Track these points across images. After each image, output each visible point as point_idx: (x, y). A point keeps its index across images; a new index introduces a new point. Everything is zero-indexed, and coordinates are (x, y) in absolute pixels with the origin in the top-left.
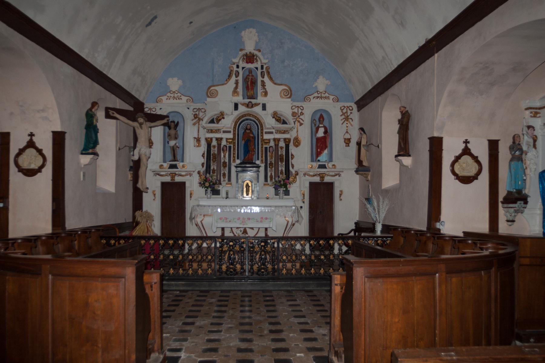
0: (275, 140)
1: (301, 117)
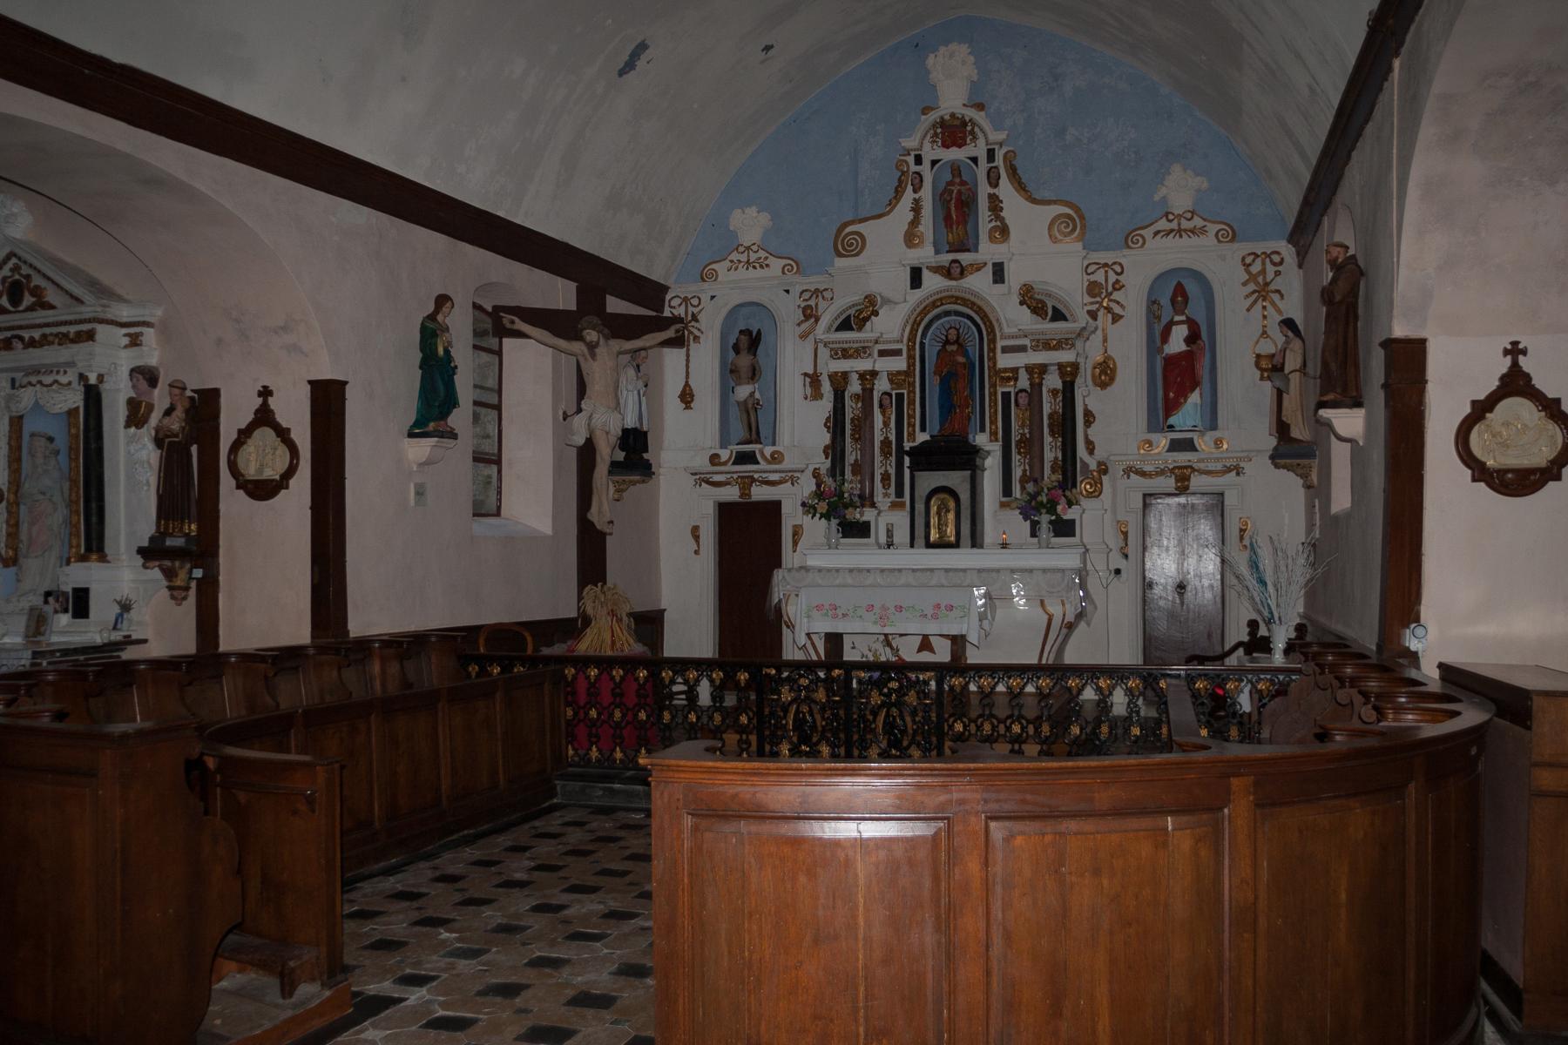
0: (1030, 369)
1: (1116, 296)
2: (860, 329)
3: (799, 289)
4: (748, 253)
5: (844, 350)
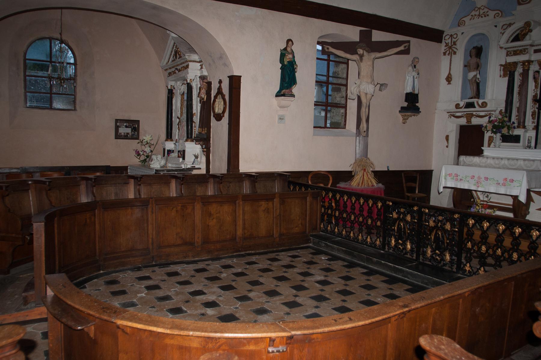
2: (522, 40)
3: (501, 24)
4: (479, 11)
5: (514, 51)
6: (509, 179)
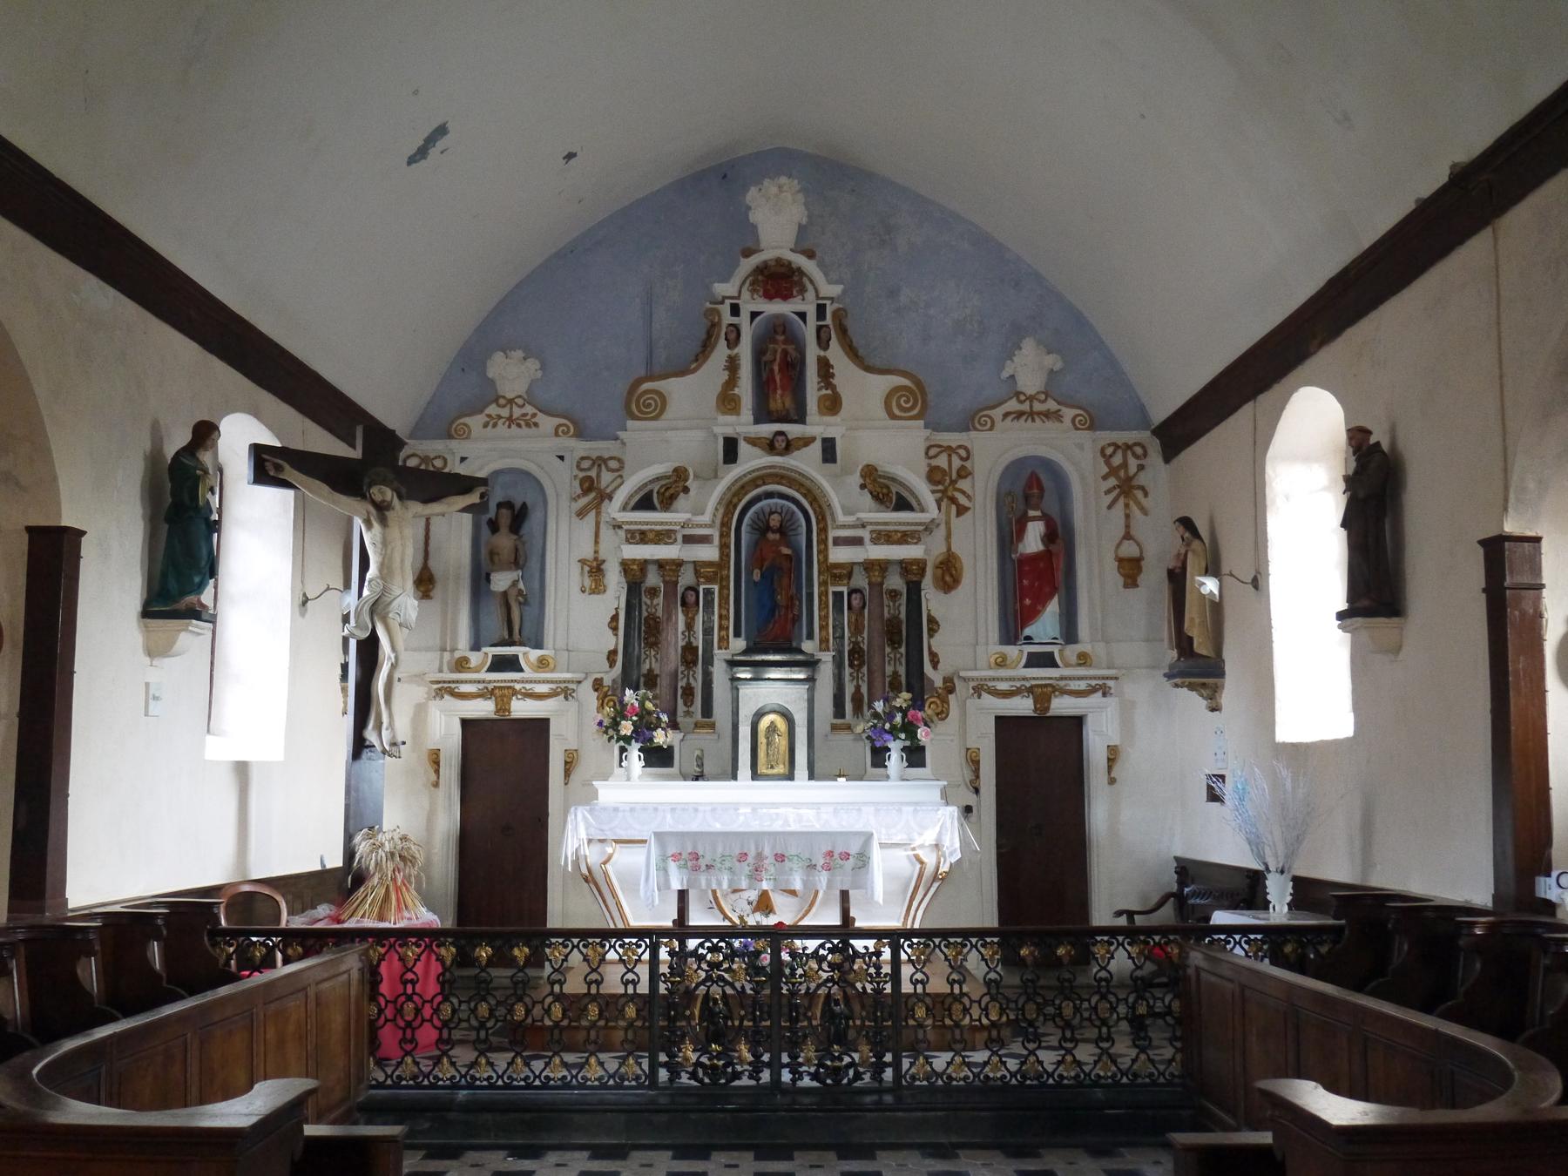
6: (839, 852)
